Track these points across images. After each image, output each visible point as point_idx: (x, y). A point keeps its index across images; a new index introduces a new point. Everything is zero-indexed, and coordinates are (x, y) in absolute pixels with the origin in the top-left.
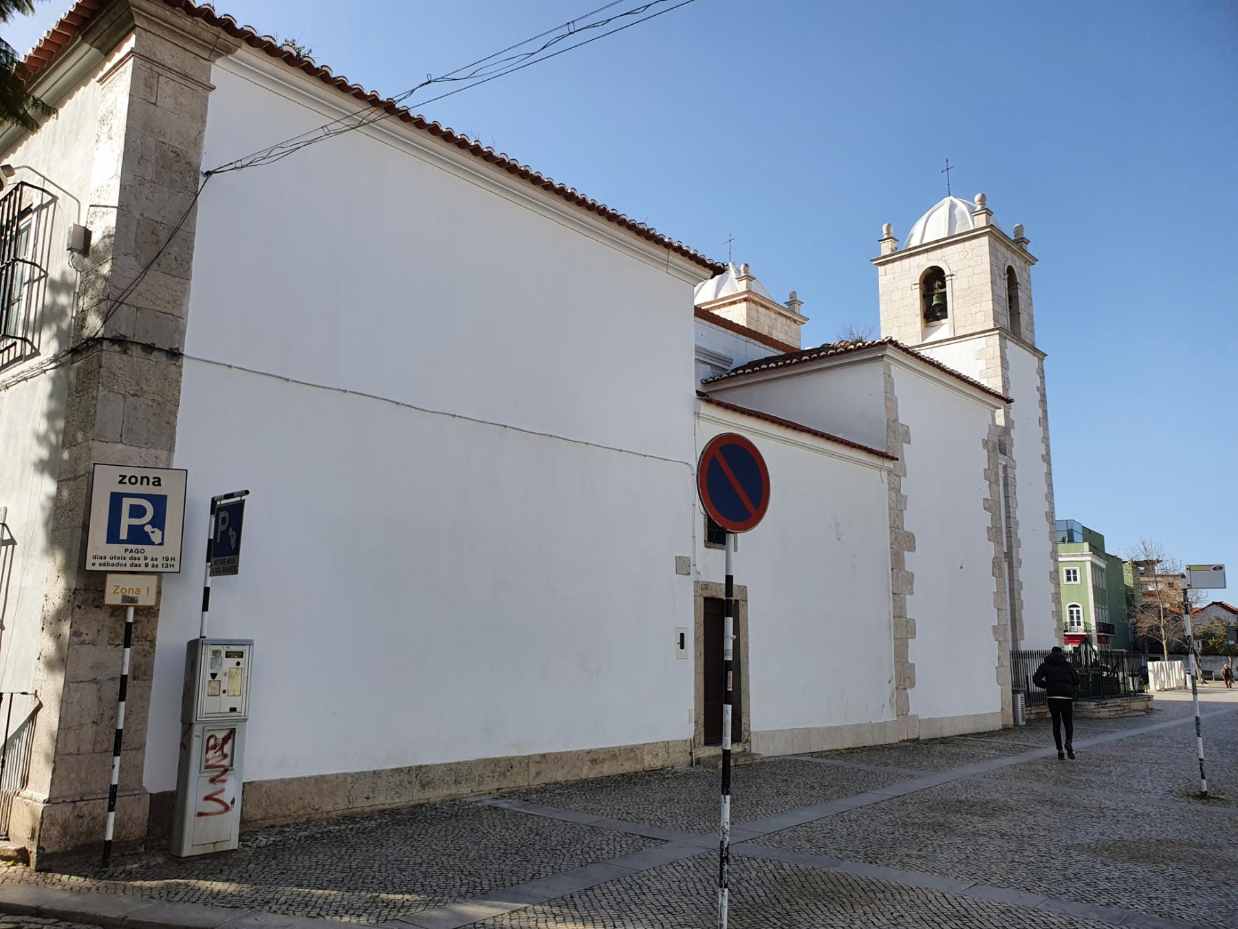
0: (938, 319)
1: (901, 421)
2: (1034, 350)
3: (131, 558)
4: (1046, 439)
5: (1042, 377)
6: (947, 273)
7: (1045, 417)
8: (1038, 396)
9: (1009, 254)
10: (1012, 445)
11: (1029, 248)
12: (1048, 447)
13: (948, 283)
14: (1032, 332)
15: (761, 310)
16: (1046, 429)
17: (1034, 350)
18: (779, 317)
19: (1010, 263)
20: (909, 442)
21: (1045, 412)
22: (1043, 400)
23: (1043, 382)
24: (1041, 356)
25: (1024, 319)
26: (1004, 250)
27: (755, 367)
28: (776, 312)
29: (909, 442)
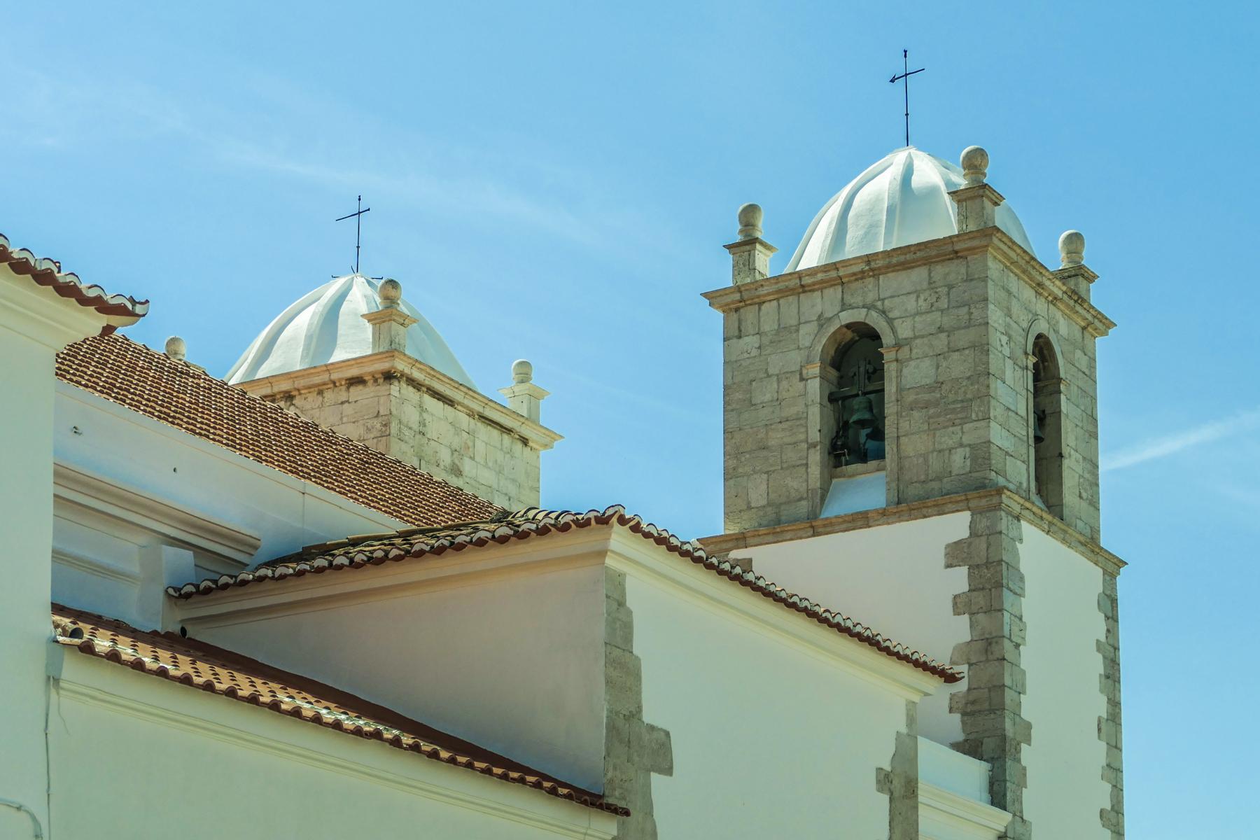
0: (863, 457)
1: (648, 717)
2: (1090, 545)
3: (188, 417)
4: (1113, 771)
5: (1112, 619)
6: (887, 339)
7: (1114, 716)
8: (1097, 665)
9: (1041, 306)
10: (1022, 784)
11: (1097, 295)
12: (1117, 789)
13: (890, 369)
14: (1094, 504)
15: (429, 401)
16: (1115, 747)
17: (1090, 545)
18: (482, 428)
19: (1042, 327)
20: (668, 771)
21: (1114, 704)
22: (1112, 675)
23: (1112, 632)
24: (1112, 566)
25: (1071, 469)
26: (1028, 293)
27: (403, 551)
28: (471, 414)
29: (668, 771)
